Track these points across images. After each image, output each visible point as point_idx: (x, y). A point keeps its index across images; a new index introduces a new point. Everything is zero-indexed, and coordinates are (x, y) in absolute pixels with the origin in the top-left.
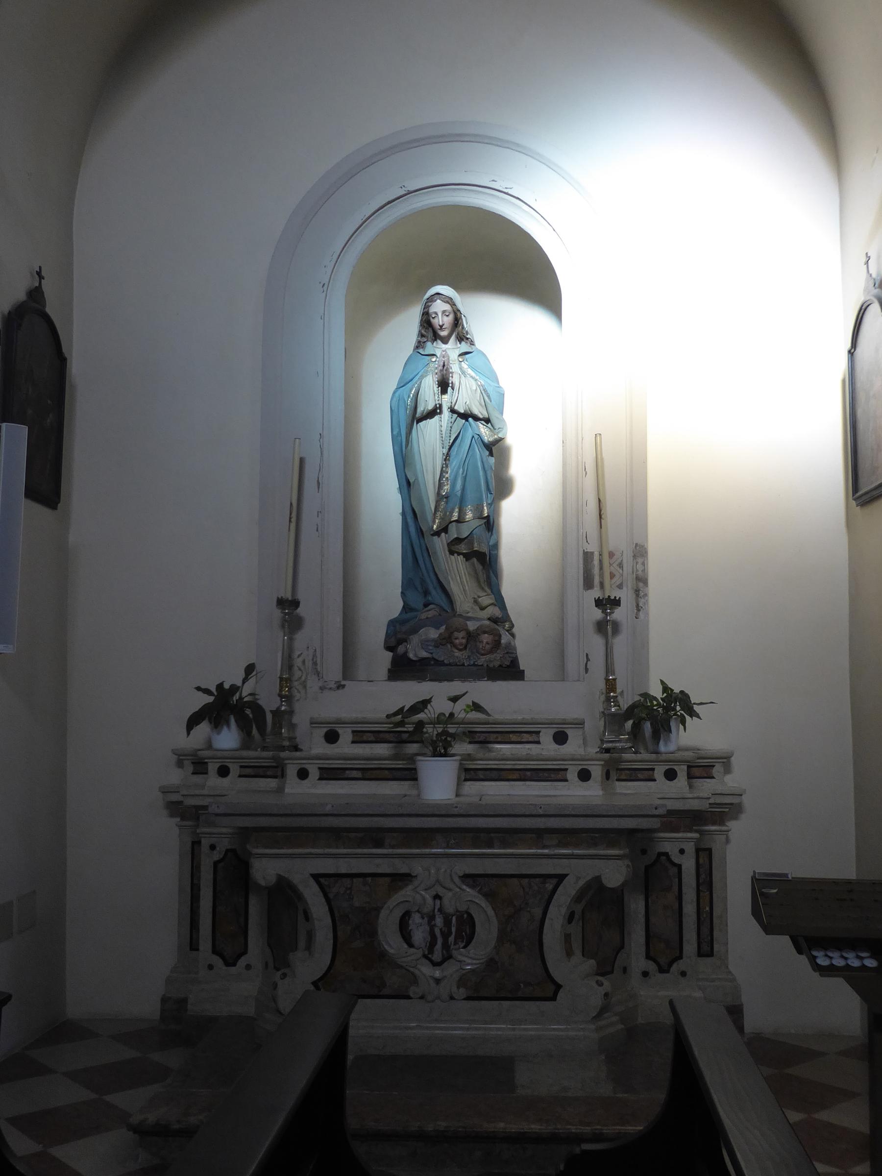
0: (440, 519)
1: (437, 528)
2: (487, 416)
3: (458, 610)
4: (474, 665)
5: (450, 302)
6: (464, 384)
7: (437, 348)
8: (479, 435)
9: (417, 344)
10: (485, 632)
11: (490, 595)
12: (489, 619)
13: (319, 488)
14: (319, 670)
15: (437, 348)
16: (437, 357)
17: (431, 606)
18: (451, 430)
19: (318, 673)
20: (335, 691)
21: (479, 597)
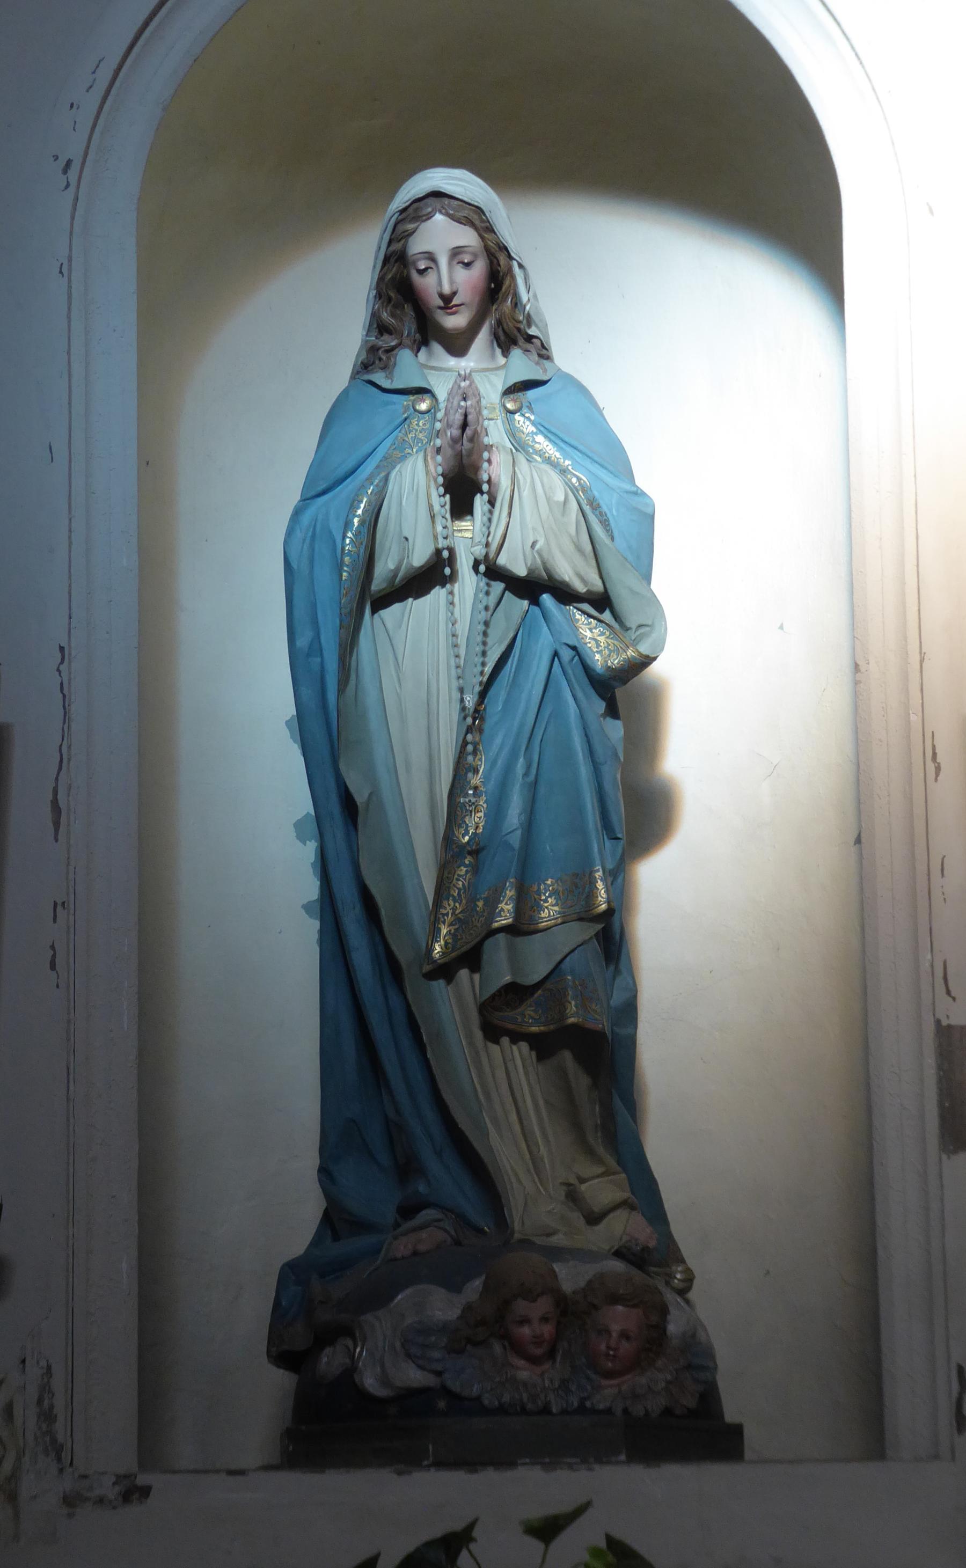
0: (451, 925)
1: (444, 954)
2: (598, 586)
3: (517, 1226)
4: (582, 1410)
5: (477, 222)
6: (529, 480)
7: (433, 368)
8: (574, 648)
9: (363, 356)
10: (614, 1299)
11: (614, 1173)
12: (618, 1254)
13: (57, 824)
14: (60, 1438)
15: (433, 368)
16: (434, 396)
17: (424, 1212)
18: (485, 634)
19: (56, 1450)
20: (114, 1508)
21: (582, 1181)
